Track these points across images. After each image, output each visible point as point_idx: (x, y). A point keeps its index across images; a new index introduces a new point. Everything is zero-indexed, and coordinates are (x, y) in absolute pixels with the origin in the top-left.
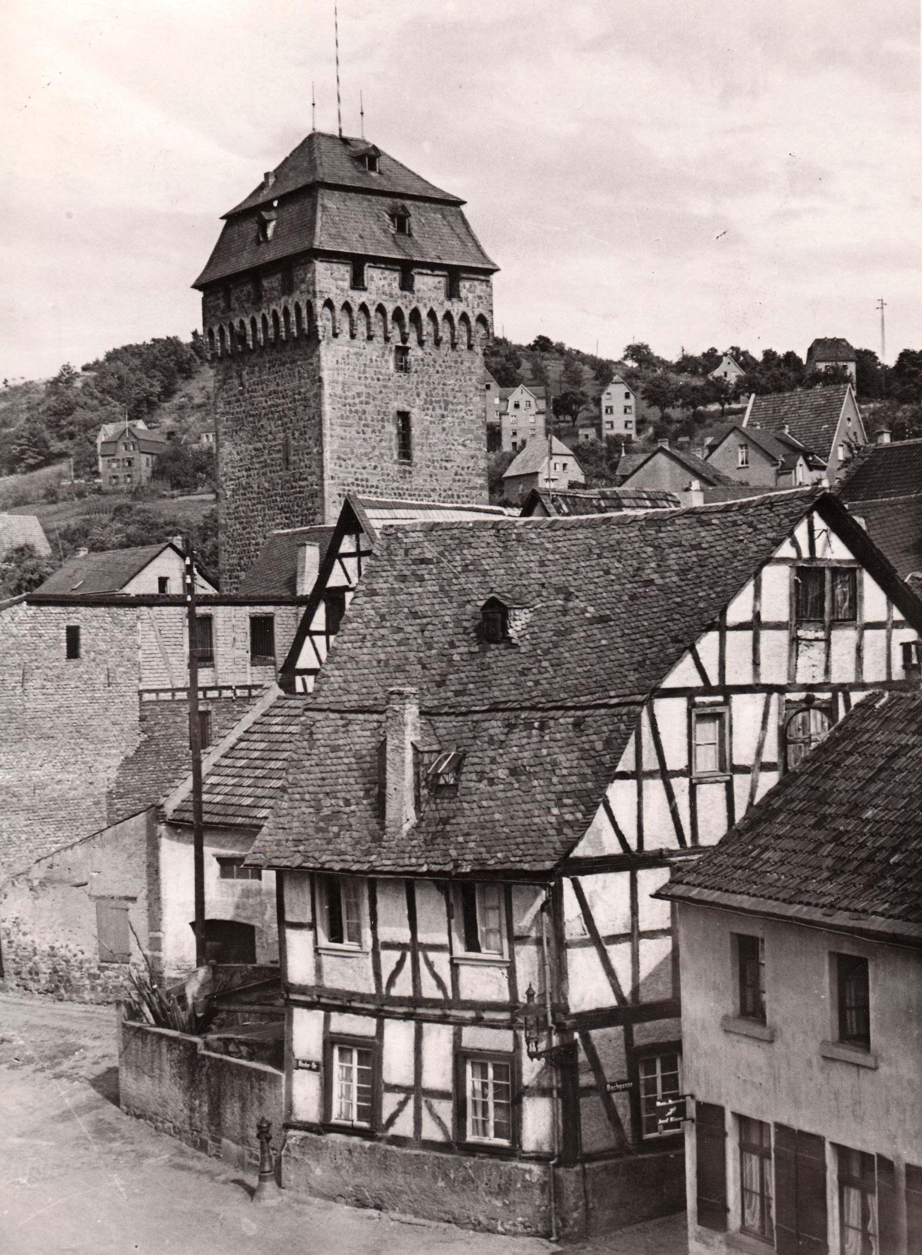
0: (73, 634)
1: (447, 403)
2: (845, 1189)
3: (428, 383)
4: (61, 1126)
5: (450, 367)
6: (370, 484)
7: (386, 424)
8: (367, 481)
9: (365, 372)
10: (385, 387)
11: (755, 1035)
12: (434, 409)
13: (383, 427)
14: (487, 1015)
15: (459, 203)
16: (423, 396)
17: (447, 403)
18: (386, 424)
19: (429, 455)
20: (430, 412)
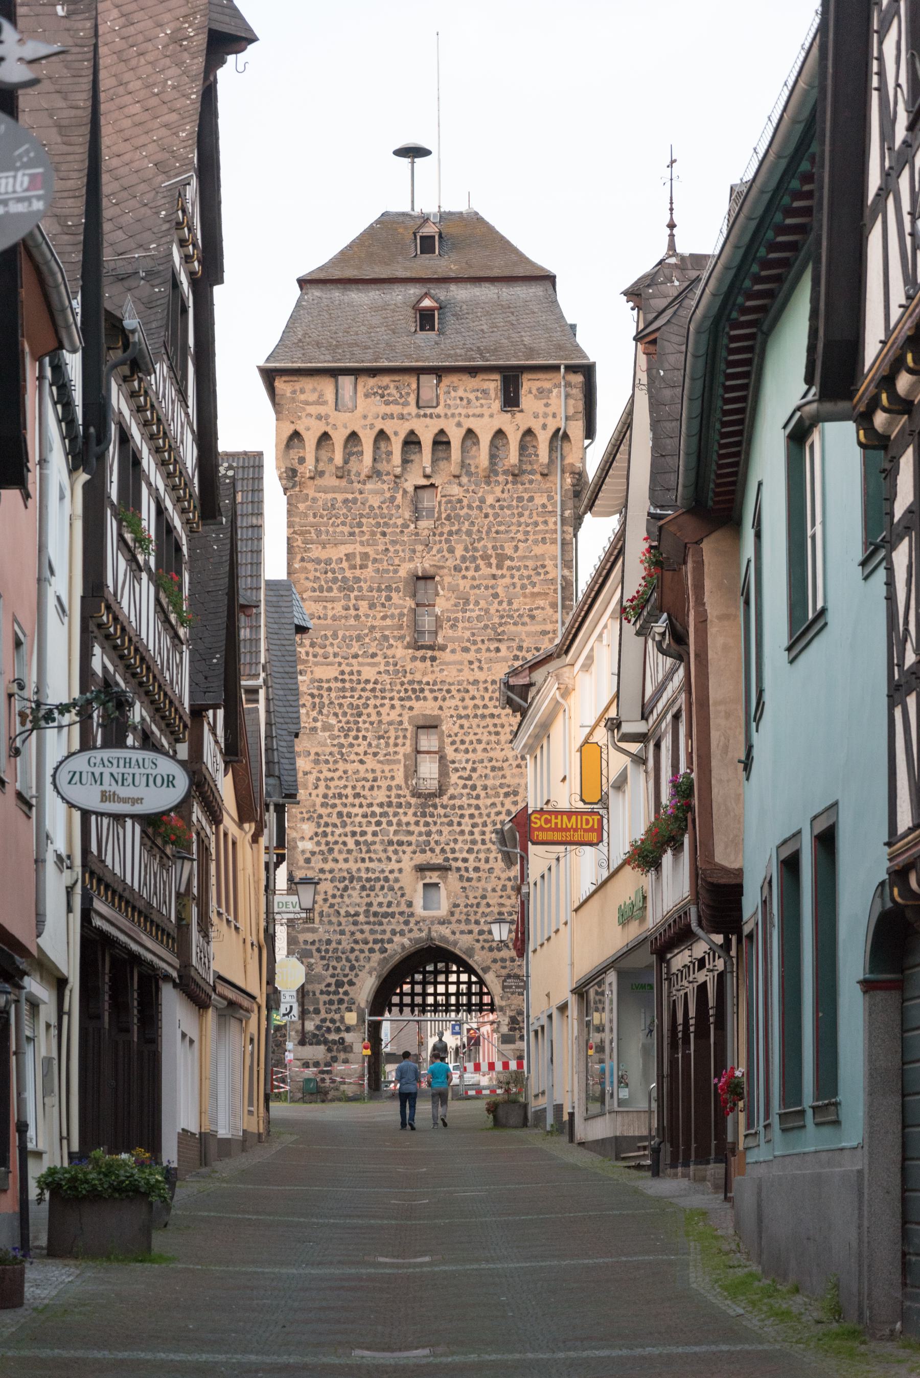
0: (536, 1096)
1: (502, 558)
2: (497, 377)
3: (469, 533)
4: (670, 1187)
5: (509, 507)
6: (363, 677)
7: (394, 595)
8: (359, 673)
9: (360, 525)
10: (394, 542)
11: (333, 396)
12: (477, 569)
13: (389, 598)
14: (65, 1142)
15: (550, 279)
16: (459, 552)
17: (502, 558)
18: (394, 595)
19: (467, 634)
20: (470, 574)
